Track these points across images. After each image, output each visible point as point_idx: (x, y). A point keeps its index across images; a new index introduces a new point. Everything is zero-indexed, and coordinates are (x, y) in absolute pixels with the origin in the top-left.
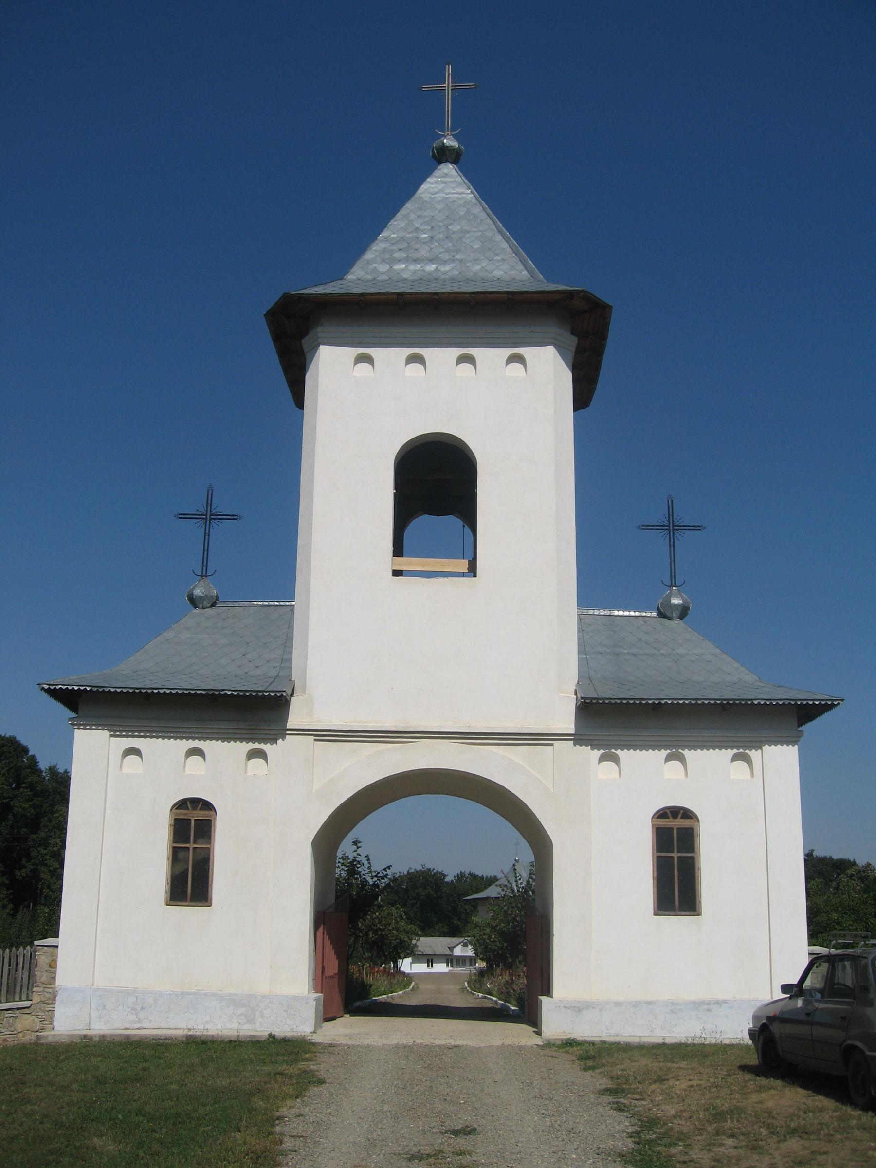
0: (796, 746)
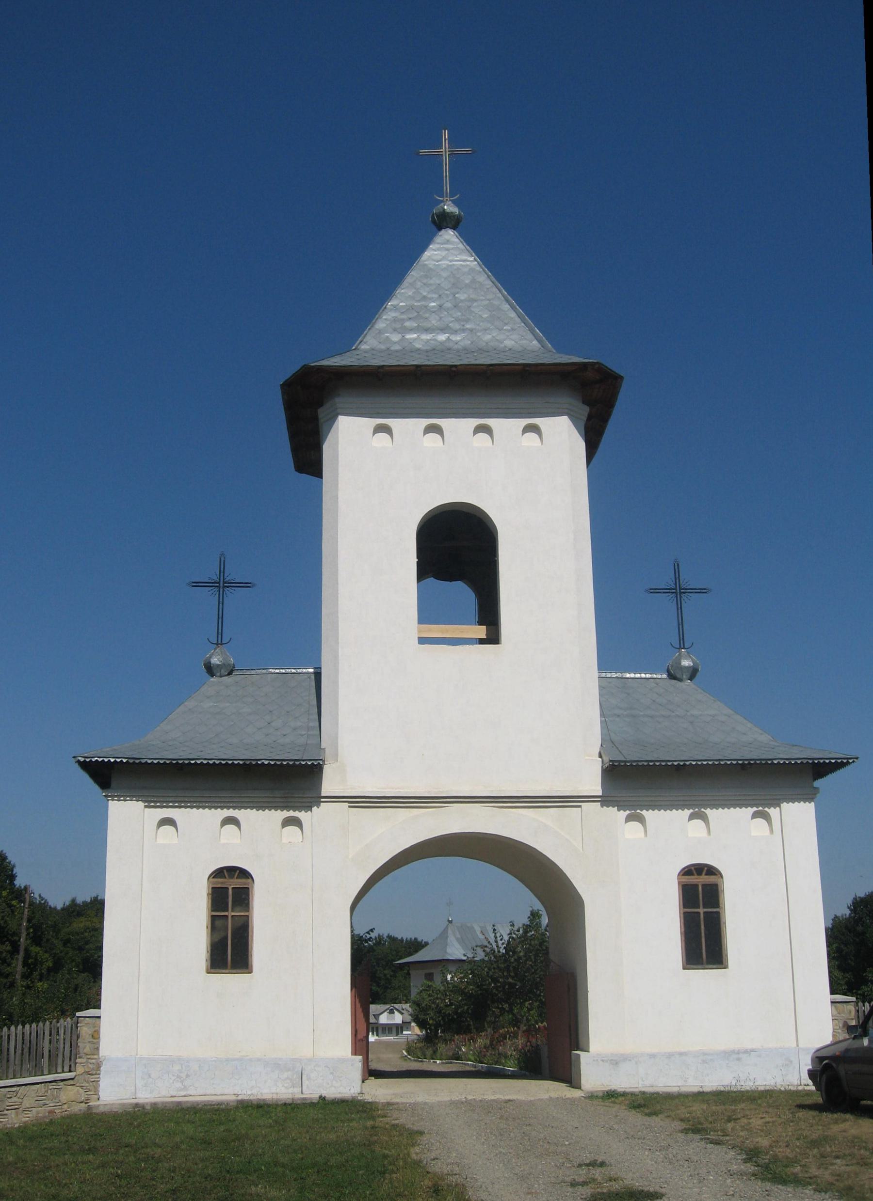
0: (813, 803)
